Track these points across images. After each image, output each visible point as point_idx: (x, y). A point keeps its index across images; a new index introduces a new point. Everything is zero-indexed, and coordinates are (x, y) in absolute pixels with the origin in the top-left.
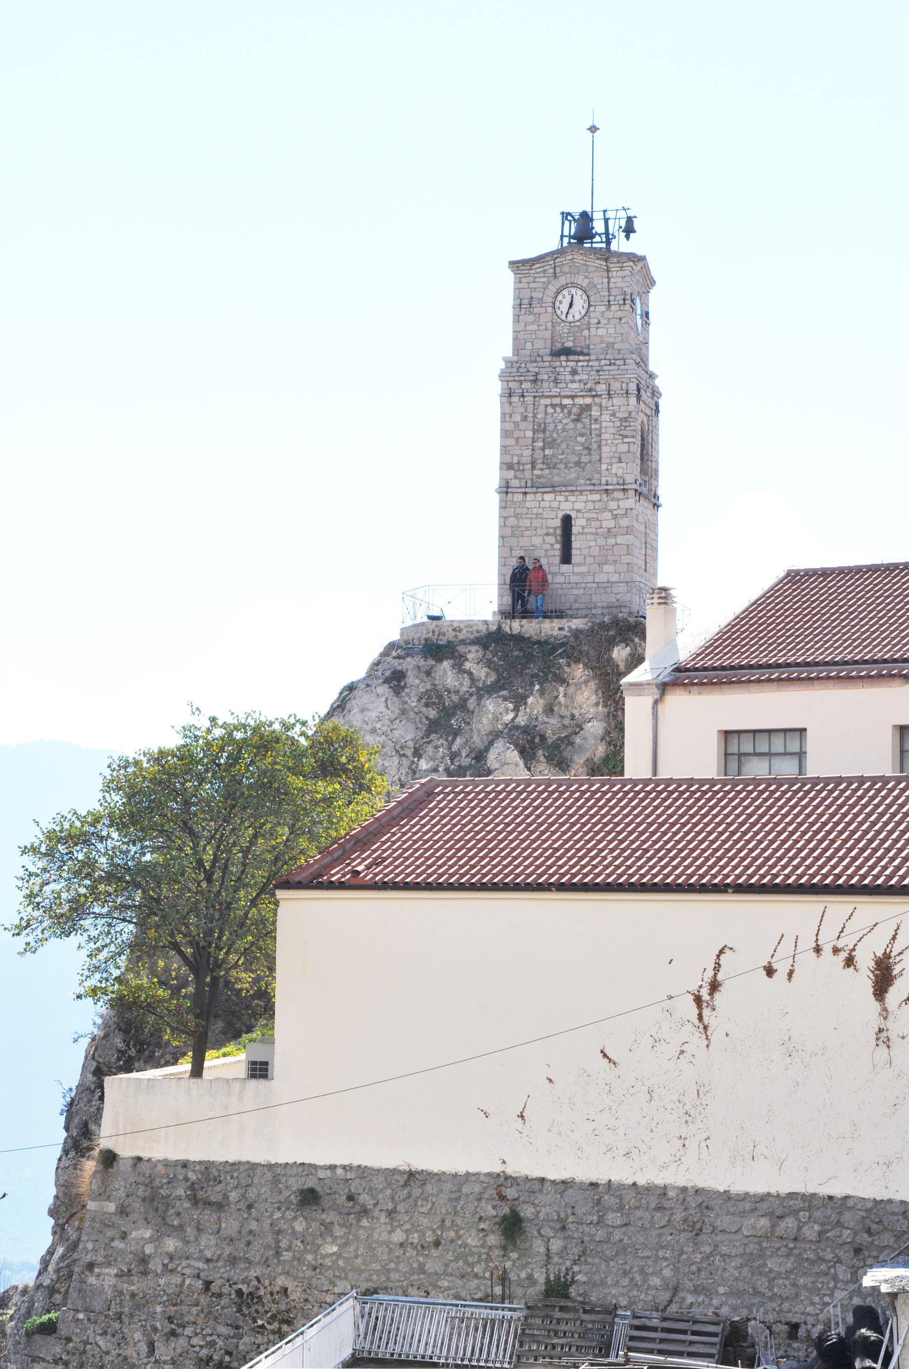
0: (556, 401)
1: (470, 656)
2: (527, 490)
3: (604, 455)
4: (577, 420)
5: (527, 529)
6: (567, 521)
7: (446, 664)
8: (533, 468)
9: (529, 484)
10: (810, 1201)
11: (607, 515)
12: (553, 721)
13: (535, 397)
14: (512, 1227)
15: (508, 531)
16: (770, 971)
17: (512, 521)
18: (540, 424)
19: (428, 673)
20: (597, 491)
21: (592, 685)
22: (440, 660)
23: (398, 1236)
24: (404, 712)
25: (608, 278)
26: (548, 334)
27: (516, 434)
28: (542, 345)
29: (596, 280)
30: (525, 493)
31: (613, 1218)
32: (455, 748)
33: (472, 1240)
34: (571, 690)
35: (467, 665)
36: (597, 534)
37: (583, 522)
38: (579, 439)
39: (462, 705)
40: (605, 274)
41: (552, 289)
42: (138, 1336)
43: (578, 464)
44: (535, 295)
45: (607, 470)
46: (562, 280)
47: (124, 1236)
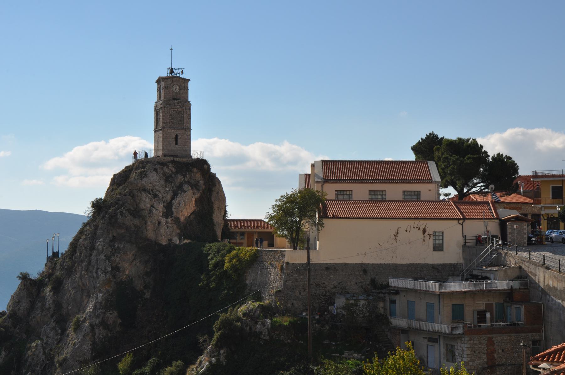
6: (177, 136)
10: (413, 264)
14: (365, 271)
16: (406, 231)
19: (162, 169)
21: (199, 173)
22: (164, 166)
23: (344, 274)
31: (381, 269)
33: (357, 273)
39: (171, 176)
41: (172, 85)
47: (292, 276)
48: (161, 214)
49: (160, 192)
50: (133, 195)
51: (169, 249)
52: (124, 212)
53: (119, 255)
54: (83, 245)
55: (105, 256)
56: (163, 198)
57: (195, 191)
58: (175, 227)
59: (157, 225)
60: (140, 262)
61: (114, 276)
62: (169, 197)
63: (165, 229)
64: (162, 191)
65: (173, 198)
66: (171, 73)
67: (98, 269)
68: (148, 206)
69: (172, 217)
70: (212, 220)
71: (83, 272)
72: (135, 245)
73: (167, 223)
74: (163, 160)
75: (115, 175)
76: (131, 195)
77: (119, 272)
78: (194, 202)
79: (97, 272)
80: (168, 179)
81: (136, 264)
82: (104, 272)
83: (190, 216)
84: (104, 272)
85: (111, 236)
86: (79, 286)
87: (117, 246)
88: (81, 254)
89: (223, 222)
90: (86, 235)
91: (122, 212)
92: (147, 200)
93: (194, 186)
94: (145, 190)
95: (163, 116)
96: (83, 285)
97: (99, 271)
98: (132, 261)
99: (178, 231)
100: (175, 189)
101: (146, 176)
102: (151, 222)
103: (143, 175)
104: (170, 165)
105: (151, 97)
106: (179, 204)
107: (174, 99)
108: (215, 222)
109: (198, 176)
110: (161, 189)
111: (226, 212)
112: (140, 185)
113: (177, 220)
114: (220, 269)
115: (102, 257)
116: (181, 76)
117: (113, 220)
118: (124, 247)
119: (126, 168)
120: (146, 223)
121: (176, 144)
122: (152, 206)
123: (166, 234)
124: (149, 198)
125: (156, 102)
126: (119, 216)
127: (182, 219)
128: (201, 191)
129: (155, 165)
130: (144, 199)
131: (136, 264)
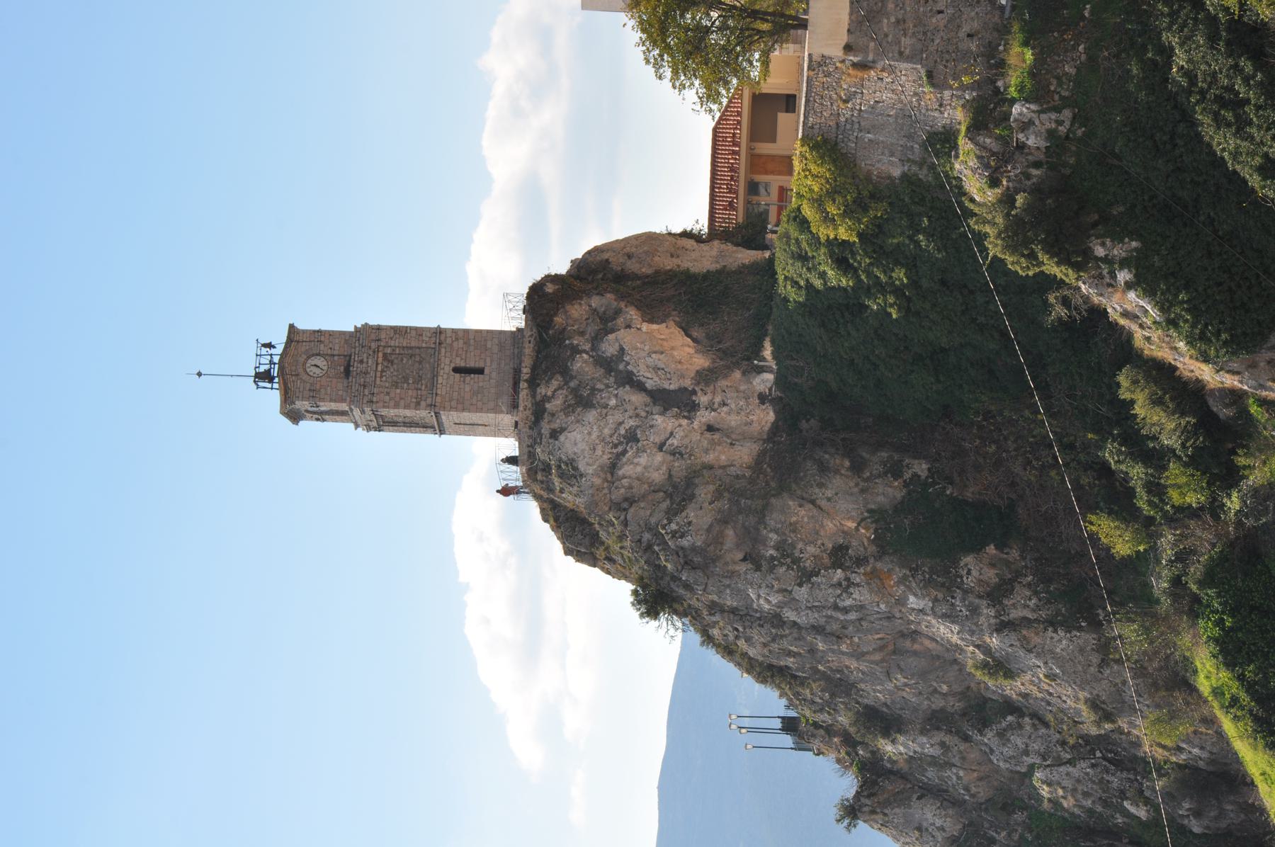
1: (543, 392)
4: (392, 362)
6: (457, 370)
7: (547, 406)
11: (455, 344)
12: (589, 329)
15: (460, 406)
17: (454, 403)
19: (553, 415)
21: (568, 307)
24: (578, 421)
32: (602, 387)
34: (570, 322)
35: (549, 393)
39: (575, 392)
41: (305, 377)
42: (934, 20)
43: (420, 363)
46: (301, 371)
48: (684, 422)
49: (621, 424)
50: (626, 499)
51: (790, 404)
52: (674, 526)
53: (800, 545)
54: (765, 645)
55: (800, 585)
56: (637, 416)
57: (620, 321)
58: (723, 383)
59: (717, 436)
60: (821, 485)
61: (860, 561)
62: (637, 399)
63: (729, 413)
64: (618, 416)
65: (639, 386)
66: (271, 380)
67: (836, 607)
68: (659, 457)
69: (694, 392)
70: (707, 276)
71: (844, 648)
72: (773, 500)
73: (711, 407)
74: (528, 413)
75: (566, 553)
76: (625, 505)
77: (847, 548)
78: (655, 327)
79: (846, 610)
80: (582, 401)
81: (829, 499)
82: (846, 590)
83: (694, 340)
84: (846, 590)
85: (742, 568)
86: (883, 660)
87: (771, 552)
88: (790, 654)
89: (716, 243)
90: (737, 637)
91: (674, 534)
92: (643, 460)
93: (606, 322)
94: (613, 467)
95: (396, 406)
96: (881, 648)
97: (841, 604)
98: (820, 508)
99: (737, 374)
100: (612, 379)
101: (571, 463)
102: (707, 451)
103: (570, 472)
104: (542, 390)
105: (340, 442)
106: (656, 369)
107: (347, 372)
108: (714, 267)
109: (577, 310)
110: (611, 419)
111: (686, 234)
112: (597, 481)
113: (706, 377)
114: (853, 254)
115: (802, 593)
116: (279, 349)
117: (697, 559)
118: (776, 531)
119: (546, 520)
120: (711, 467)
121: (480, 371)
122: (661, 447)
123: (744, 409)
124: (637, 455)
125: (357, 426)
126: (685, 542)
127: (701, 362)
128: (622, 305)
129: (540, 434)
130: (639, 469)
131: (829, 499)
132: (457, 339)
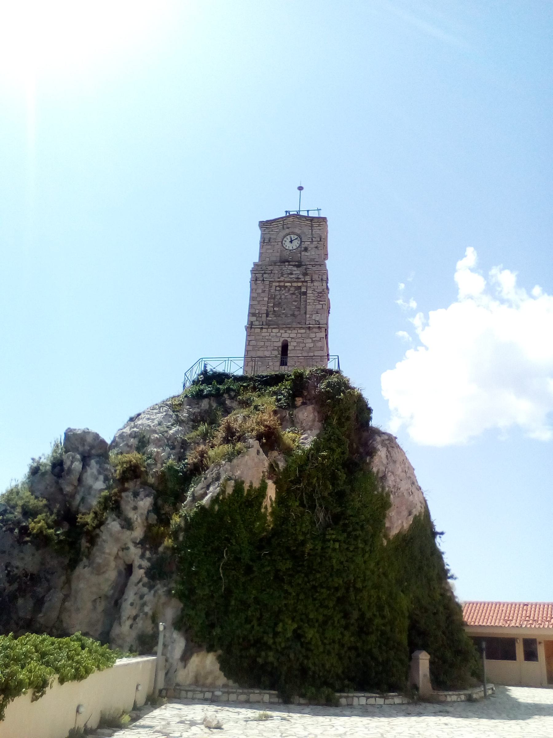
0: (282, 284)
2: (263, 326)
3: (307, 310)
5: (262, 347)
8: (267, 316)
9: (264, 323)
13: (270, 281)
18: (272, 295)
20: (304, 328)
25: (312, 230)
26: (278, 254)
27: (258, 299)
28: (275, 257)
29: (305, 231)
30: (262, 328)
36: (302, 350)
37: (295, 344)
38: (294, 303)
40: (310, 228)
44: (272, 237)
45: (310, 317)
46: (287, 231)
132: (313, 342)
